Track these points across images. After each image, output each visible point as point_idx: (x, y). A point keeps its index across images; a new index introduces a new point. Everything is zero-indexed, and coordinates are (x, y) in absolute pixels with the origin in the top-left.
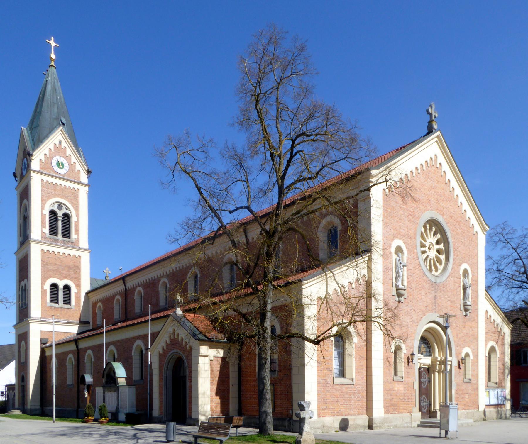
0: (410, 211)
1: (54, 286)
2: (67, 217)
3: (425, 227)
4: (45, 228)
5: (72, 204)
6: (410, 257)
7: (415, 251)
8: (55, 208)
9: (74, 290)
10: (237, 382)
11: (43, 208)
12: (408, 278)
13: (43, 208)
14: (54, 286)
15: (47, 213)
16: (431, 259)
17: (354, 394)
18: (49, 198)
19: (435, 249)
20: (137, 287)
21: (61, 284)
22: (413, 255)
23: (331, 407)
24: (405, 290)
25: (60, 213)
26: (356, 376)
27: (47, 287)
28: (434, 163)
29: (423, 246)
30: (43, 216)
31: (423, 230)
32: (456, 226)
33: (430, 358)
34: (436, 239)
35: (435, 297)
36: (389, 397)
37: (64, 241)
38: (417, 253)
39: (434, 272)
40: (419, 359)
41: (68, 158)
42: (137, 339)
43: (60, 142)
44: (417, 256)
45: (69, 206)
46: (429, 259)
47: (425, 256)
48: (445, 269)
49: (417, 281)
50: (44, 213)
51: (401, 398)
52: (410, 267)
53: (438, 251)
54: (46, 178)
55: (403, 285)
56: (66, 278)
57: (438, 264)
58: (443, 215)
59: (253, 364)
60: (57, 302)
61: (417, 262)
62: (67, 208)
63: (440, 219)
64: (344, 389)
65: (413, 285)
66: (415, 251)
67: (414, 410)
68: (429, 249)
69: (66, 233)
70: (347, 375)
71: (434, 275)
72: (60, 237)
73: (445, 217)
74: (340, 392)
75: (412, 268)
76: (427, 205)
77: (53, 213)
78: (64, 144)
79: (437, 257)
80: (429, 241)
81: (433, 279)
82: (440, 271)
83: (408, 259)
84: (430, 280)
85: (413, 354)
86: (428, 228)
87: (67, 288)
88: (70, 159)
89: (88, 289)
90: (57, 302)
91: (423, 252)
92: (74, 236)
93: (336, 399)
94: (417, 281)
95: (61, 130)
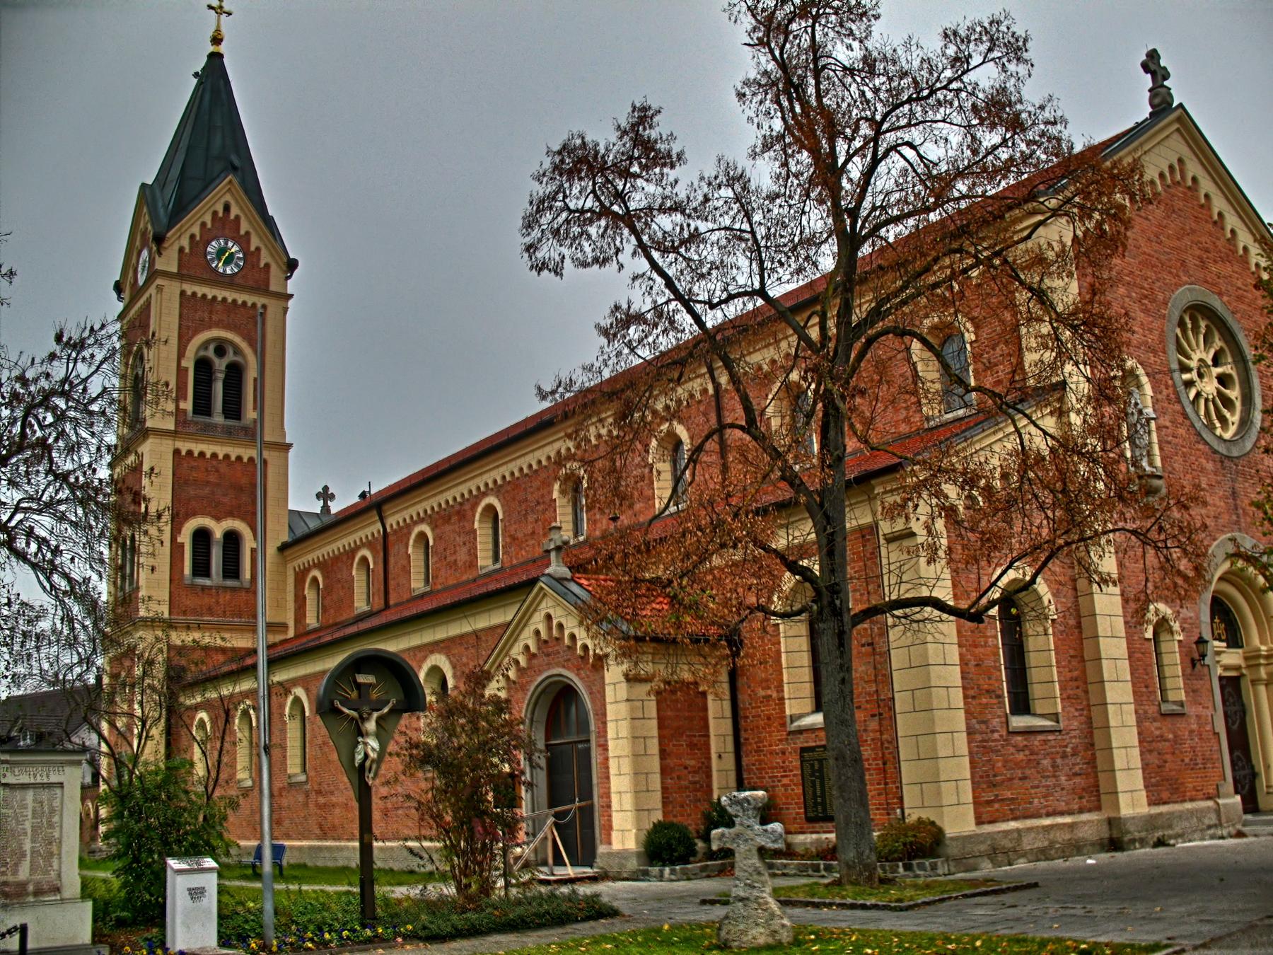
0: (1143, 288)
1: (202, 536)
2: (235, 373)
3: (1182, 324)
4: (185, 399)
5: (252, 344)
6: (1159, 397)
7: (1170, 382)
8: (211, 353)
9: (249, 543)
10: (730, 747)
11: (181, 354)
12: (1161, 449)
13: (181, 354)
14: (202, 536)
15: (189, 364)
16: (1207, 400)
17: (1064, 756)
18: (196, 332)
19: (1214, 375)
20: (415, 523)
21: (218, 530)
22: (1165, 392)
23: (1008, 794)
24: (1160, 477)
25: (220, 365)
26: (1063, 708)
27: (185, 538)
28: (1178, 178)
29: (1185, 369)
30: (181, 372)
31: (1178, 331)
32: (1255, 318)
33: (1240, 651)
34: (1212, 352)
35: (1234, 494)
36: (1154, 760)
37: (229, 428)
38: (1174, 386)
39: (1219, 431)
40: (1218, 653)
41: (243, 241)
42: (432, 652)
43: (227, 208)
44: (1177, 393)
45: (244, 345)
46: (1202, 402)
47: (1192, 394)
48: (1245, 422)
49: (1184, 455)
50: (184, 364)
51: (1187, 760)
52: (1161, 421)
53: (1223, 380)
54: (189, 289)
55: (1151, 464)
56: (231, 514)
57: (1225, 412)
58: (1220, 294)
59: (775, 695)
60: (207, 574)
61: (1177, 407)
62: (237, 351)
63: (1216, 303)
64: (1036, 743)
65: (1176, 465)
66: (1170, 382)
67: (1222, 790)
68: (1201, 376)
69: (233, 408)
70: (1038, 707)
71: (1220, 438)
72: (218, 419)
73: (1225, 299)
74: (1027, 752)
75: (1168, 424)
76: (1181, 274)
77: (203, 366)
78: (234, 211)
79: (1219, 392)
80: (1196, 356)
81: (1222, 449)
82: (1232, 429)
83: (1155, 401)
84: (1215, 452)
85: (1201, 641)
86: (1189, 326)
87: (232, 539)
88: (248, 242)
89: (285, 537)
90: (207, 574)
91: (1189, 384)
92: (250, 414)
93: (1019, 773)
94: (1184, 455)
95: (230, 182)
